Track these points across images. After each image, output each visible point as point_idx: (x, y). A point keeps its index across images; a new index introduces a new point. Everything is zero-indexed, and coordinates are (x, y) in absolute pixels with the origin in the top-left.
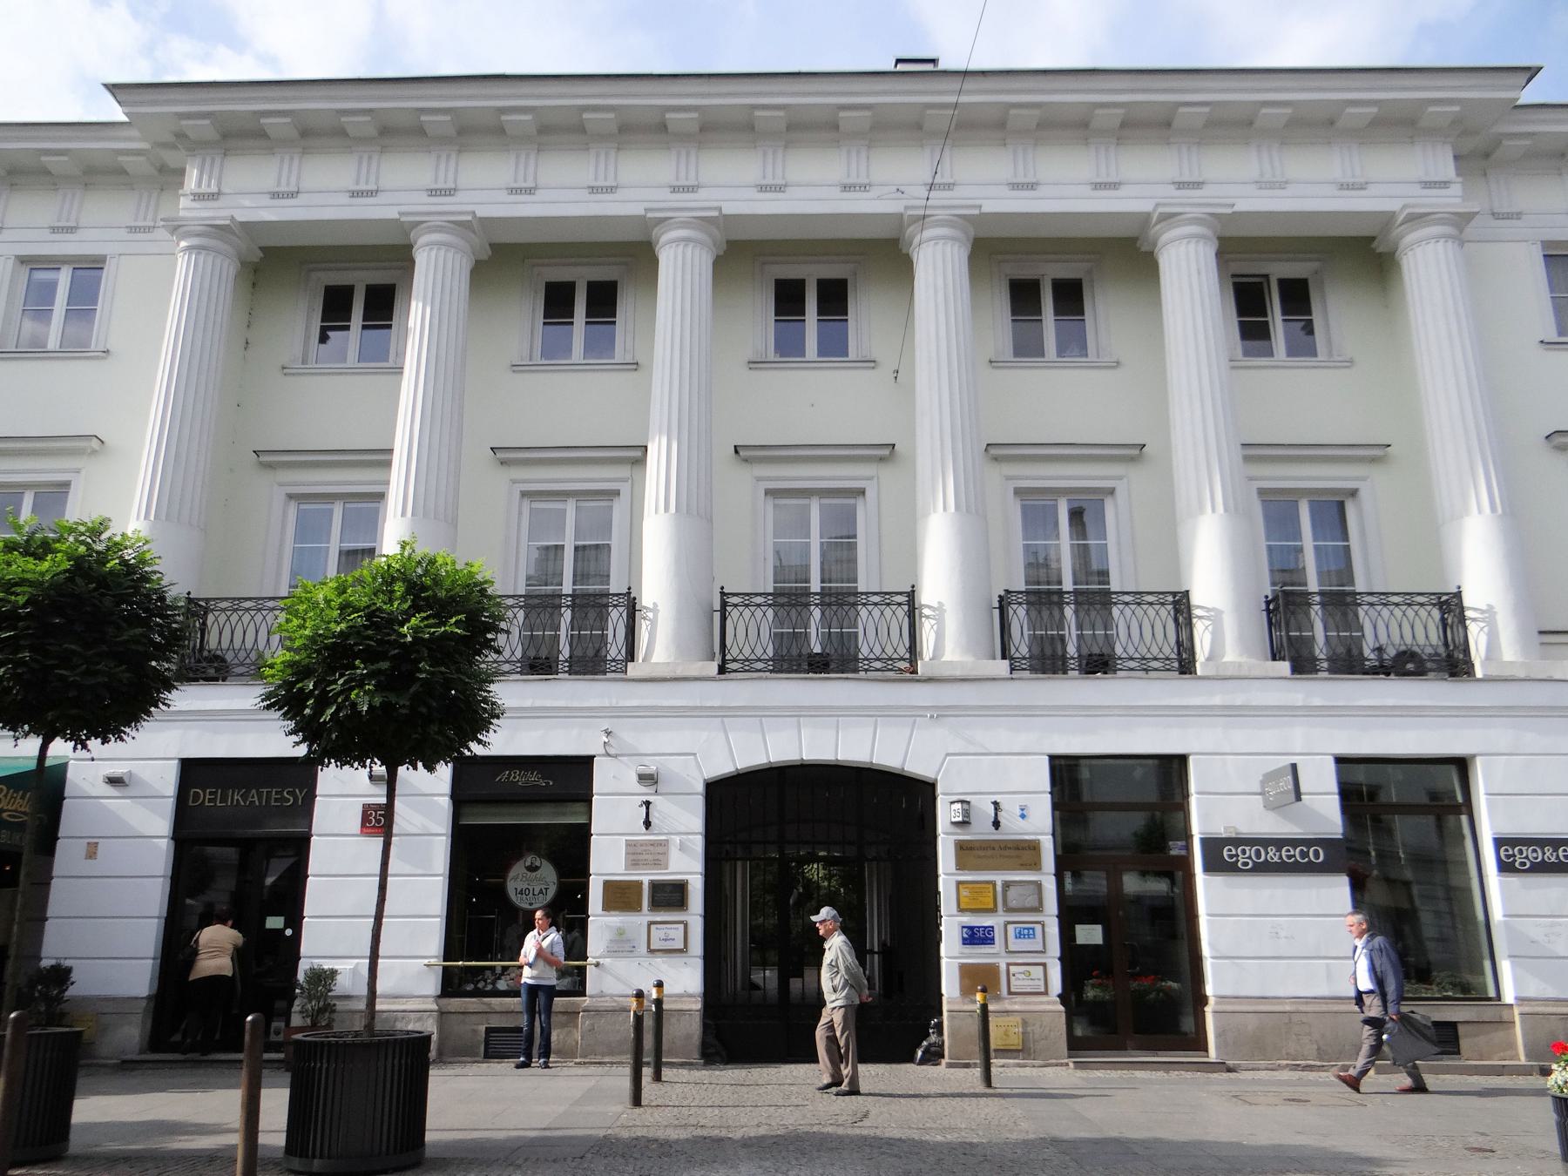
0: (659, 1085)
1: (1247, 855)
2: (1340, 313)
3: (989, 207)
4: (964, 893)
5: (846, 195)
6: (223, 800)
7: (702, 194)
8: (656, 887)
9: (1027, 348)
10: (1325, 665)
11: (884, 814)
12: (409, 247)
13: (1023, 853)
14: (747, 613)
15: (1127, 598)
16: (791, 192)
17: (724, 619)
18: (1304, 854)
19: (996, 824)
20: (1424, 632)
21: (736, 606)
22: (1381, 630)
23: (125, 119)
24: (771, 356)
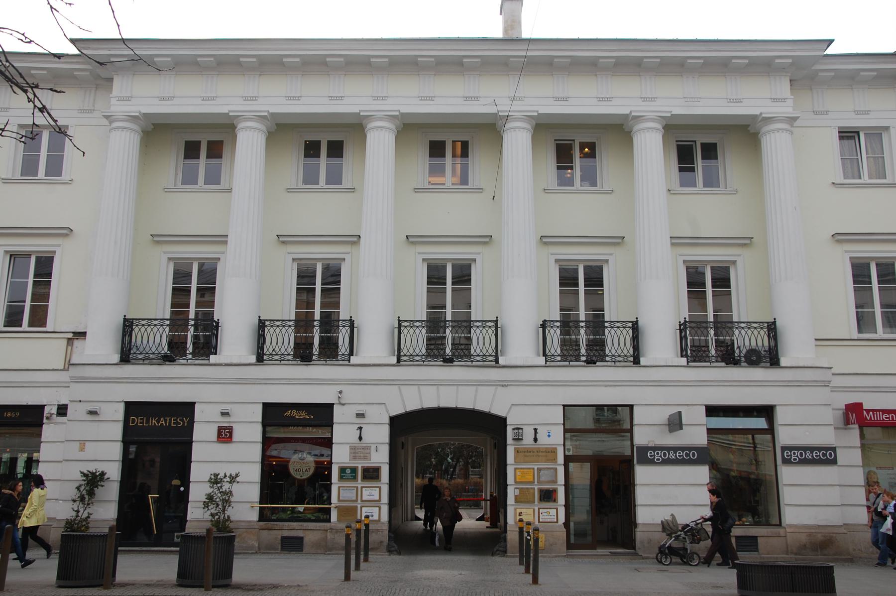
2: (731, 165)
4: (518, 473)
5: (466, 103)
6: (147, 422)
11: (486, 430)
14: (412, 331)
19: (536, 440)
20: (760, 340)
22: (743, 340)
23: (77, 52)
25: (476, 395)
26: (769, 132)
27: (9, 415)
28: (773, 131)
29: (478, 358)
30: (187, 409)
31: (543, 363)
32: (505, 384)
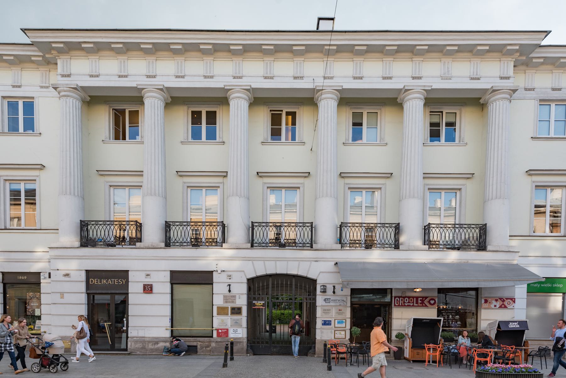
0: (113, 361)
6: (101, 282)
7: (244, 79)
8: (233, 309)
9: (196, 136)
10: (364, 245)
12: (142, 97)
16: (393, 80)
17: (253, 229)
24: (190, 139)
25: (310, 266)
26: (495, 100)
27: (20, 278)
28: (498, 99)
29: (301, 245)
30: (124, 274)
31: (340, 248)
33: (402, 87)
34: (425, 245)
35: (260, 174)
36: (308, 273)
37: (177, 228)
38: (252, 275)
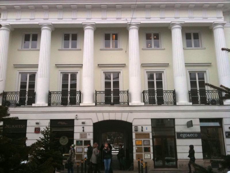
1: (184, 136)
2: (204, 40)
3: (142, 22)
4: (137, 142)
9: (107, 46)
13: (147, 135)
14: (100, 95)
15: (168, 92)
18: (194, 135)
19: (142, 130)
21: (98, 93)
26: (216, 28)
29: (122, 103)
30: (24, 122)
32: (131, 112)
33: (213, 22)
34: (190, 102)
35: (99, 66)
36: (98, 120)
37: (55, 95)
38: (96, 121)
